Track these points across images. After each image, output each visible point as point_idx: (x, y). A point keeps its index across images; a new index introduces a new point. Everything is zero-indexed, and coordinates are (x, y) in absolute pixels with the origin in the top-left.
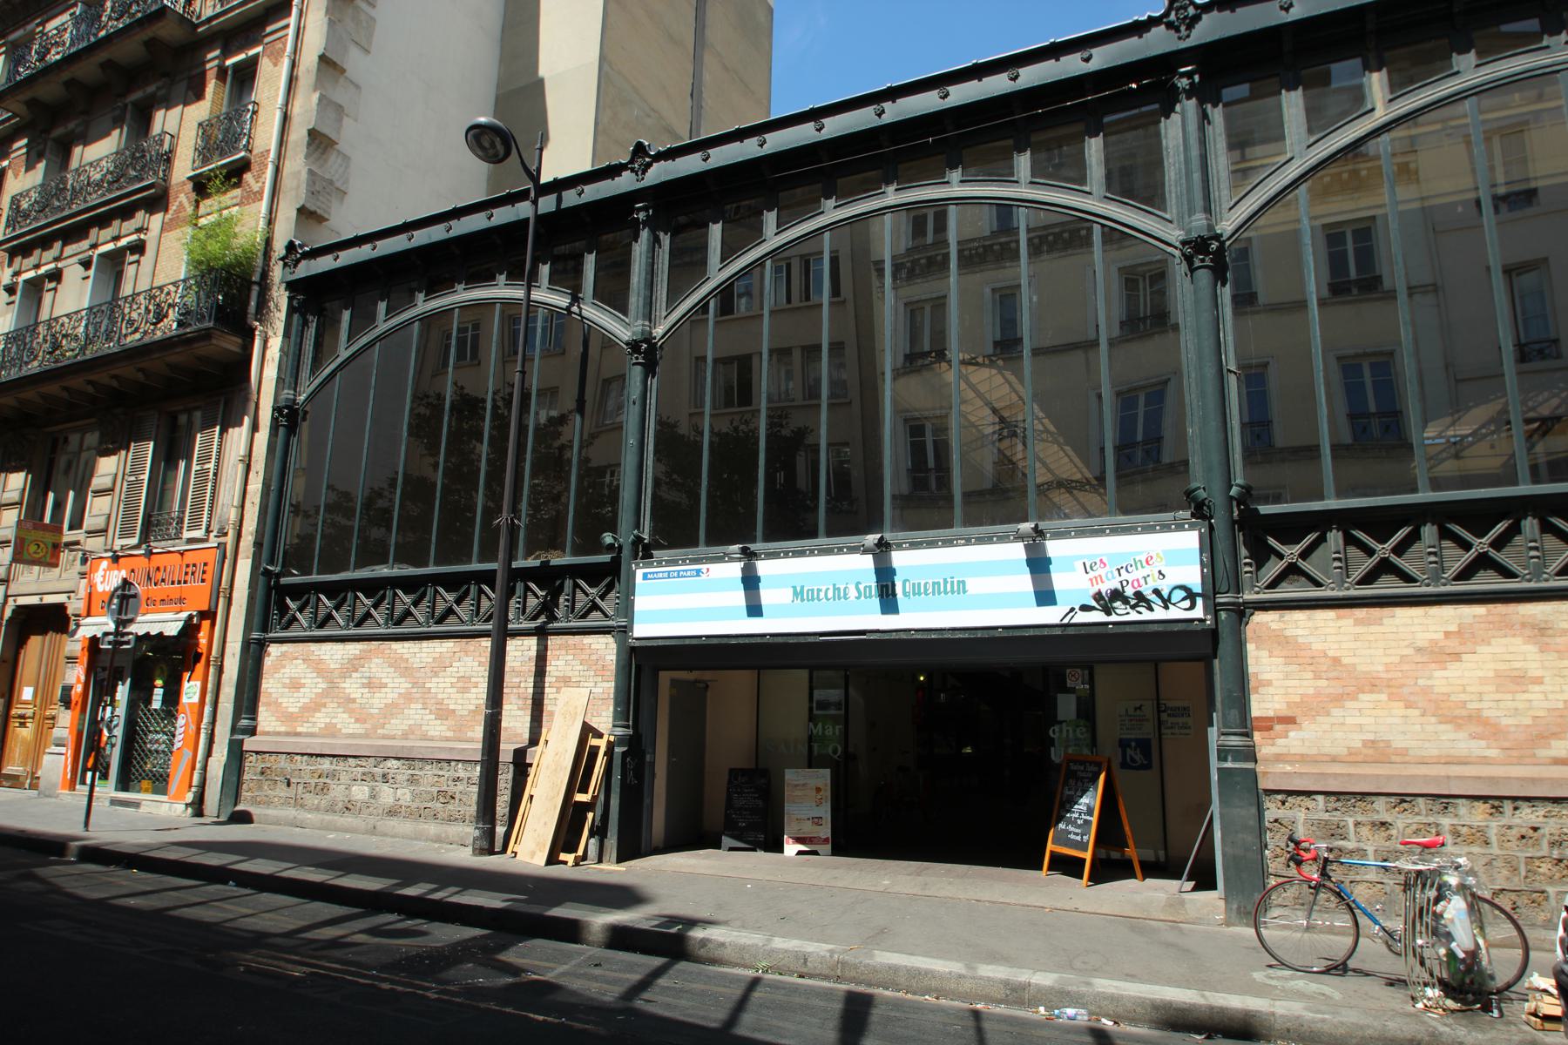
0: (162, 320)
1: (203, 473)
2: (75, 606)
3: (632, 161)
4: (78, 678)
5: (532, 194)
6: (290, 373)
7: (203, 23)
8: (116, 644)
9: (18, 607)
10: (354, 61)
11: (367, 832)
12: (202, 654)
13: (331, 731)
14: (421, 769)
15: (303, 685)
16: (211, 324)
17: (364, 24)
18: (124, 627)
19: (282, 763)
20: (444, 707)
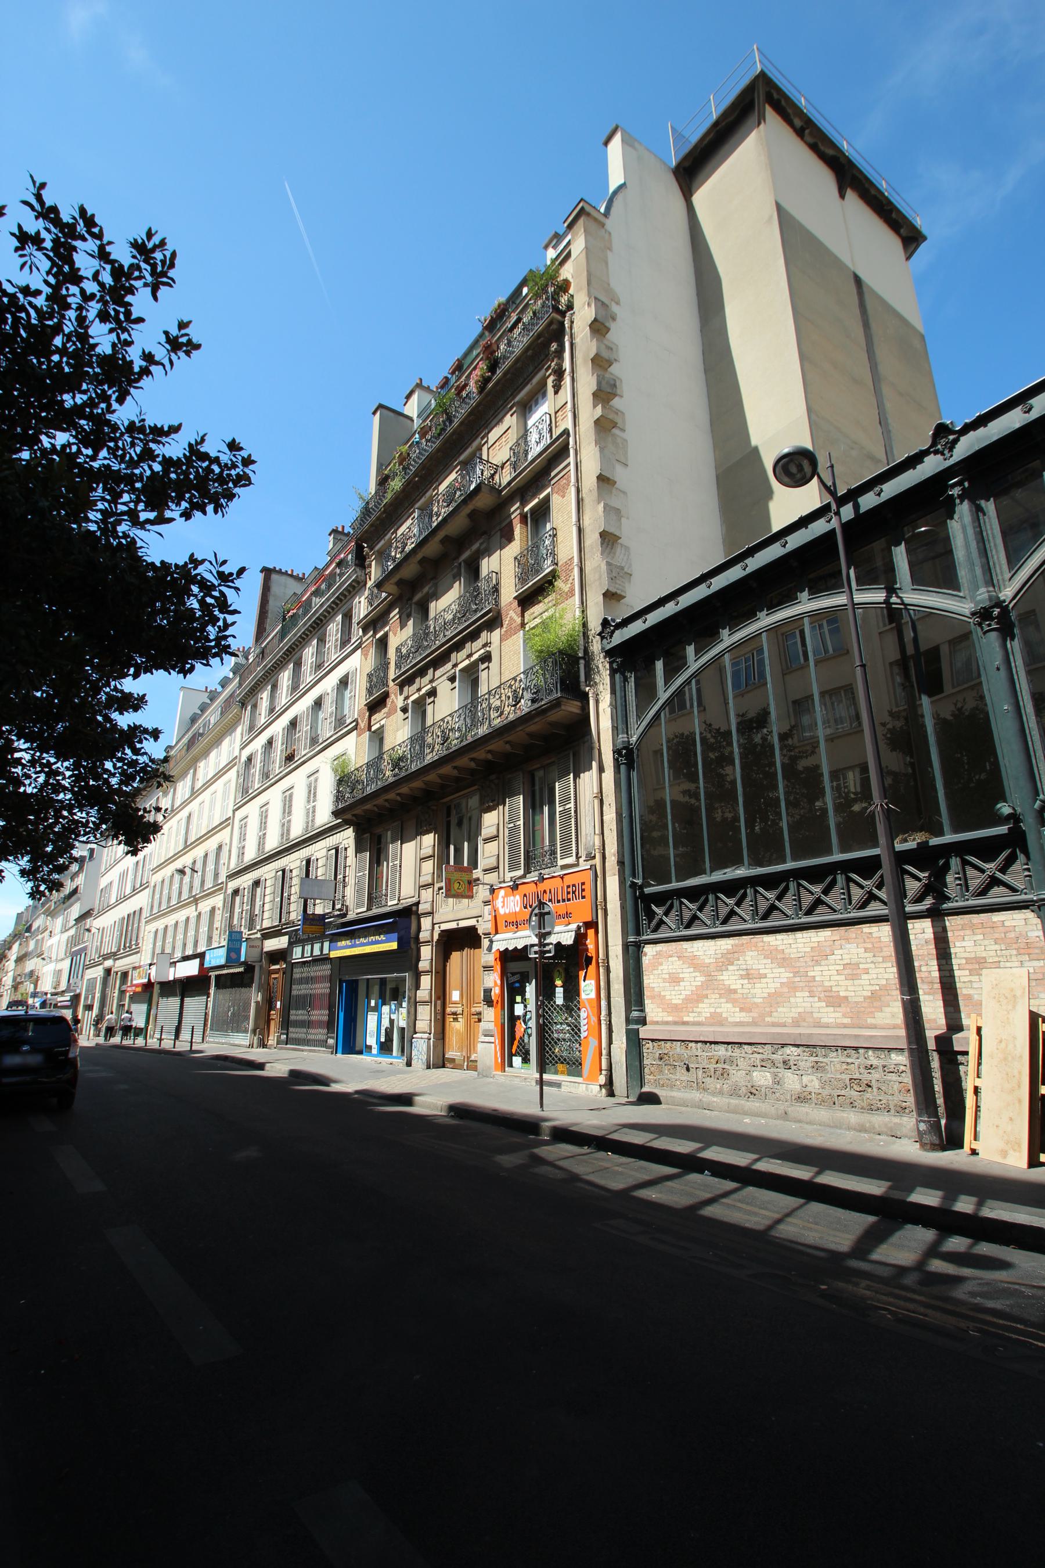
0: (520, 701)
1: (566, 812)
2: (484, 927)
3: (934, 444)
4: (495, 982)
5: (834, 507)
6: (621, 722)
7: (505, 487)
8: (542, 953)
9: (442, 931)
10: (620, 475)
11: (778, 1118)
12: (592, 957)
13: (717, 1019)
14: (825, 1056)
15: (683, 980)
16: (559, 695)
17: (621, 445)
18: (545, 939)
19: (678, 1049)
20: (833, 994)
